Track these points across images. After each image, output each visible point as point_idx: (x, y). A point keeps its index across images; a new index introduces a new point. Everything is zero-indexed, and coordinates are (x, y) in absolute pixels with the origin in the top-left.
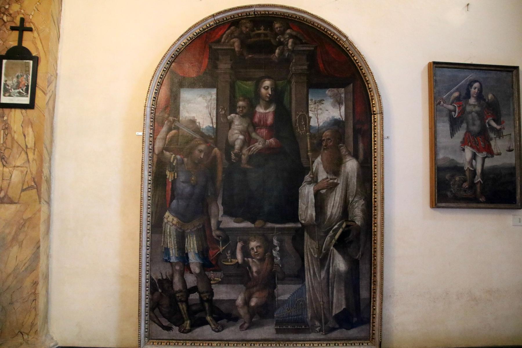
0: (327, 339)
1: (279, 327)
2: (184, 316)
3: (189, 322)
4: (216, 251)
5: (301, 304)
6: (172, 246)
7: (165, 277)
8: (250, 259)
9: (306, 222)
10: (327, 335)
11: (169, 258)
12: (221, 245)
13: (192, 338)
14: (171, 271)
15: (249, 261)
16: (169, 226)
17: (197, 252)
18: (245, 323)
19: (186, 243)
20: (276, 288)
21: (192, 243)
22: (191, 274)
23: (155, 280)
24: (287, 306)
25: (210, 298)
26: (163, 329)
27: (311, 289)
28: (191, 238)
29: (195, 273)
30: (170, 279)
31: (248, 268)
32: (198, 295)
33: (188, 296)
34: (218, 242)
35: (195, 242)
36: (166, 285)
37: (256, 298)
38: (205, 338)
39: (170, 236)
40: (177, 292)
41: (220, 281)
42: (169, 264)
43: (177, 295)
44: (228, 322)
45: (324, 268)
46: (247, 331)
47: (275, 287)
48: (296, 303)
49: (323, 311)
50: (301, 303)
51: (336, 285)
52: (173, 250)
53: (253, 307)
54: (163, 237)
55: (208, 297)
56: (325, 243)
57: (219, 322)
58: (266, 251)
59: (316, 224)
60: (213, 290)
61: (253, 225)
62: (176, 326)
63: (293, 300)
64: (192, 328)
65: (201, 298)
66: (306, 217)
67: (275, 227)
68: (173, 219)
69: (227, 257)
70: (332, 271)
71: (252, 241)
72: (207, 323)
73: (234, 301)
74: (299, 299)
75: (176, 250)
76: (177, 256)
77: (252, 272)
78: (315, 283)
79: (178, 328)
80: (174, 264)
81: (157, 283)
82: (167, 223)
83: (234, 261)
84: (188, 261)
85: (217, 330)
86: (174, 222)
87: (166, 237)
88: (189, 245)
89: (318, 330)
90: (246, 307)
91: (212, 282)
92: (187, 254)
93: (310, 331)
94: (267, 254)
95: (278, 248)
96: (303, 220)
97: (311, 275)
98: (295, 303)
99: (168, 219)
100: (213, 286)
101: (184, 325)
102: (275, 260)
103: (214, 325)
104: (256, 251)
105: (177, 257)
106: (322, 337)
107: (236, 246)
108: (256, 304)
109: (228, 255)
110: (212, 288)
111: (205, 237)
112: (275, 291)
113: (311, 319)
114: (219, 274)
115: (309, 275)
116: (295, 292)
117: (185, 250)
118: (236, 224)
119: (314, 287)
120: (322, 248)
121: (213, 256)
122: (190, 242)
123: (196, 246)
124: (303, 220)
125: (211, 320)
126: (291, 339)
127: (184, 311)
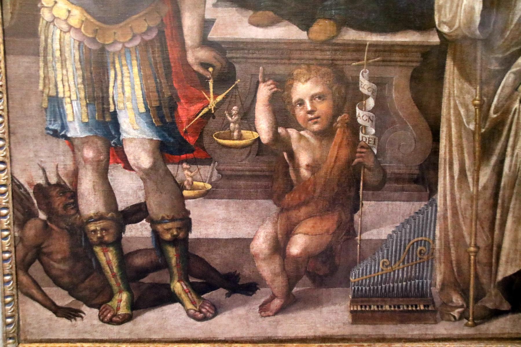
0: (478, 336)
1: (359, 309)
2: (113, 282)
3: (124, 296)
4: (200, 105)
5: (421, 251)
6: (70, 91)
7: (53, 180)
8: (293, 133)
9: (454, 29)
10: (478, 327)
11: (64, 127)
12: (211, 90)
13: (135, 337)
14: (70, 163)
15: (289, 137)
16: (58, 32)
17: (142, 110)
18: (274, 297)
19: (111, 84)
20: (358, 209)
21: (127, 83)
22: (127, 171)
23: (26, 186)
24: (383, 254)
25: (181, 235)
26: (57, 316)
27: (449, 214)
28: (125, 68)
29: (139, 168)
30: (68, 185)
31: (285, 154)
32: (150, 229)
33: (122, 230)
34: (203, 83)
35: (137, 81)
36: (58, 202)
37: (306, 234)
38: (168, 335)
39: (63, 62)
40: (90, 220)
41: (208, 191)
42: (63, 144)
43: (92, 227)
44: (228, 295)
45: (488, 159)
46: (279, 317)
47: (356, 208)
48: (407, 248)
49: (475, 269)
50: (419, 248)
51: (515, 204)
52: (75, 104)
53: (295, 258)
54: (41, 64)
55: (175, 233)
56: (499, 91)
57: (204, 296)
58: (337, 111)
59: (481, 37)
60: (188, 213)
61: (305, 33)
62: (91, 306)
63: (401, 240)
64: (134, 312)
65: (156, 234)
66: (454, 17)
67: (366, 41)
68: (69, 12)
69: (229, 123)
70: (510, 167)
71: (300, 81)
72: (173, 298)
73: (246, 242)
74: (416, 239)
75: (84, 103)
76: (86, 120)
77: (297, 168)
78: (460, 199)
79: (96, 311)
80: (76, 142)
81: (32, 195)
82: (53, 21)
83: (249, 136)
84: (119, 134)
85: (200, 315)
86: (74, 21)
87: (50, 65)
88: (120, 90)
89: (457, 316)
90: (277, 260)
91: (185, 193)
92: (114, 115)
93: (438, 316)
94: (339, 119)
95: (371, 103)
96: (445, 23)
97: (452, 177)
98: (405, 248)
99: (55, 12)
100: (189, 204)
101: (114, 303)
102: (361, 135)
103: (193, 303)
104: (309, 108)
105: (86, 124)
106: (466, 331)
107: (256, 92)
108: (305, 250)
109: (233, 119)
110: (187, 208)
111: (168, 67)
112: (356, 217)
113: (442, 289)
114: (206, 171)
115: (448, 178)
116: (408, 221)
117: (109, 104)
118: (254, 28)
119: (459, 208)
120: (490, 106)
121: (190, 121)
122: (122, 81)
123: (141, 92)
124: (445, 23)
125: (183, 289)
126: (389, 337)
127: (111, 269)
